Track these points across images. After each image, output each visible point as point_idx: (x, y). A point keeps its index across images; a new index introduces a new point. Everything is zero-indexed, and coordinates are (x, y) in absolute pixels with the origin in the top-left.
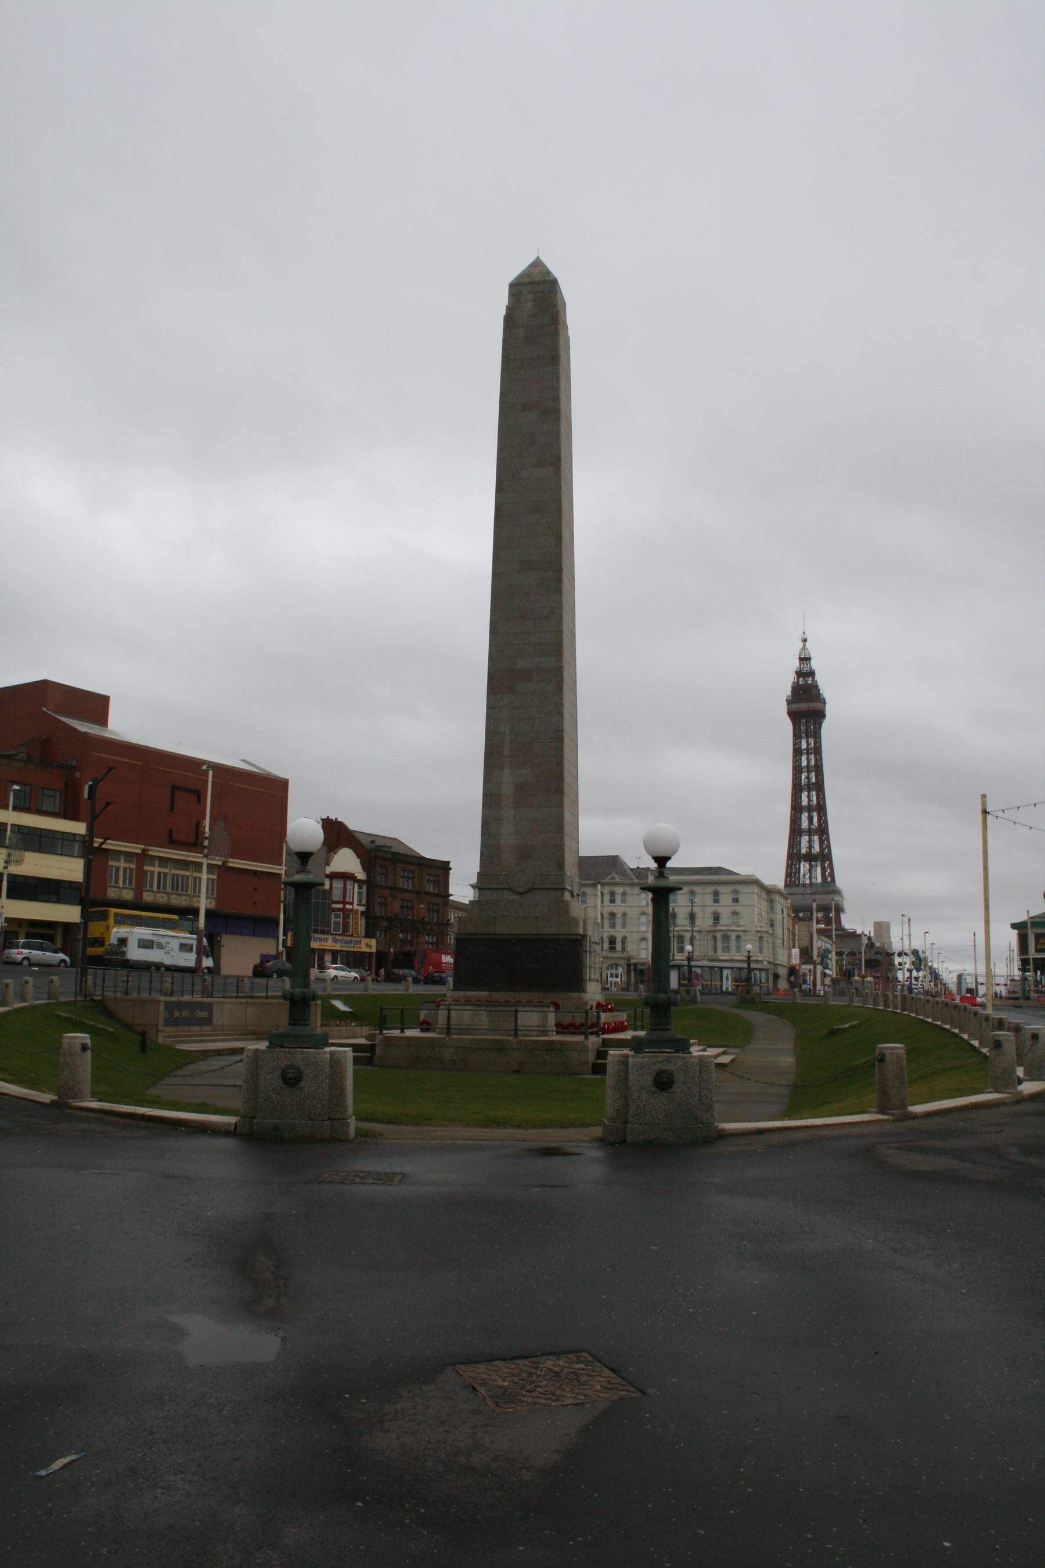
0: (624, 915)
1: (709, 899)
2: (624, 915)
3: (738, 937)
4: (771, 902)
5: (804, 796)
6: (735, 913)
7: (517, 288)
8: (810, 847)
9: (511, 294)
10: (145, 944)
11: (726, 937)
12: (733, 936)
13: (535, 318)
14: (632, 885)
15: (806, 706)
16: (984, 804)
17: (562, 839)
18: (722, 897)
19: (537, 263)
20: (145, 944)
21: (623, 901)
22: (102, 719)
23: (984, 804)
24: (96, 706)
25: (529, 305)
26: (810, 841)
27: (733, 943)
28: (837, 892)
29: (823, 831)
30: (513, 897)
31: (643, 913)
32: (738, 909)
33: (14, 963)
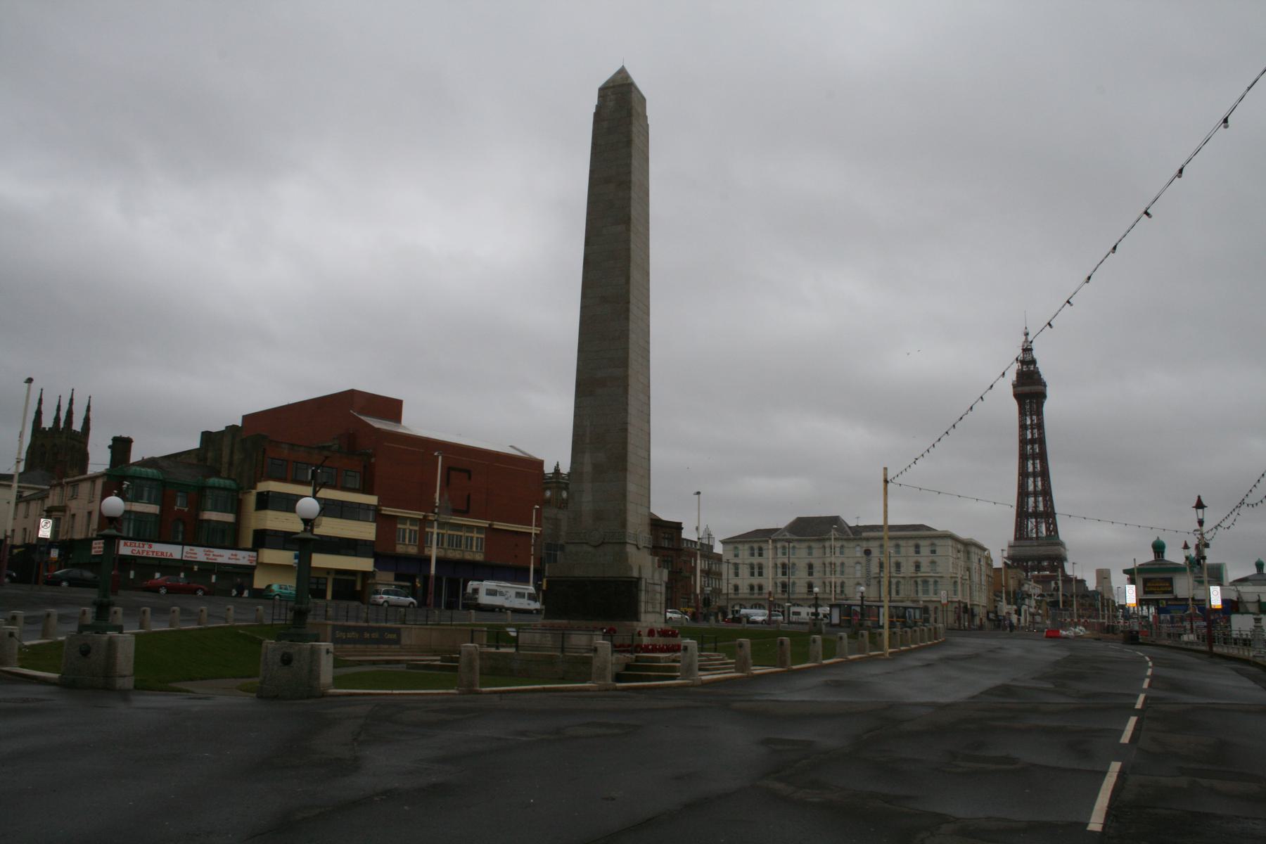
0: (842, 564)
1: (912, 550)
2: (842, 564)
3: (936, 582)
4: (968, 553)
5: (1030, 463)
6: (933, 562)
7: (604, 91)
8: (1036, 506)
9: (600, 96)
10: (491, 593)
11: (925, 582)
12: (931, 580)
13: (619, 118)
14: (848, 540)
15: (1030, 389)
16: (885, 475)
17: (625, 506)
18: (922, 549)
19: (622, 72)
20: (491, 593)
21: (841, 553)
22: (397, 417)
23: (885, 475)
24: (392, 408)
25: (611, 104)
26: (1036, 502)
27: (931, 588)
28: (1061, 544)
29: (1046, 493)
30: (590, 549)
31: (858, 563)
32: (936, 559)
33: (378, 605)
